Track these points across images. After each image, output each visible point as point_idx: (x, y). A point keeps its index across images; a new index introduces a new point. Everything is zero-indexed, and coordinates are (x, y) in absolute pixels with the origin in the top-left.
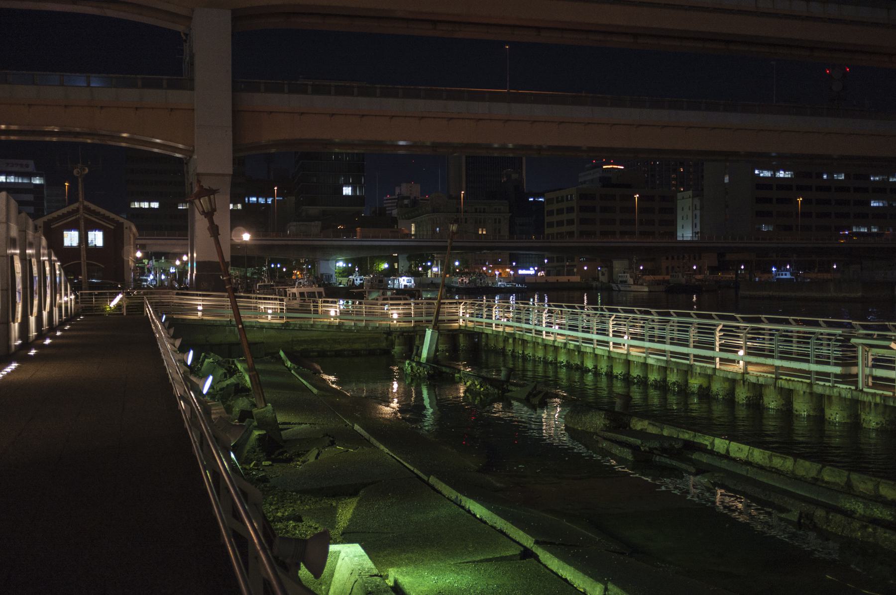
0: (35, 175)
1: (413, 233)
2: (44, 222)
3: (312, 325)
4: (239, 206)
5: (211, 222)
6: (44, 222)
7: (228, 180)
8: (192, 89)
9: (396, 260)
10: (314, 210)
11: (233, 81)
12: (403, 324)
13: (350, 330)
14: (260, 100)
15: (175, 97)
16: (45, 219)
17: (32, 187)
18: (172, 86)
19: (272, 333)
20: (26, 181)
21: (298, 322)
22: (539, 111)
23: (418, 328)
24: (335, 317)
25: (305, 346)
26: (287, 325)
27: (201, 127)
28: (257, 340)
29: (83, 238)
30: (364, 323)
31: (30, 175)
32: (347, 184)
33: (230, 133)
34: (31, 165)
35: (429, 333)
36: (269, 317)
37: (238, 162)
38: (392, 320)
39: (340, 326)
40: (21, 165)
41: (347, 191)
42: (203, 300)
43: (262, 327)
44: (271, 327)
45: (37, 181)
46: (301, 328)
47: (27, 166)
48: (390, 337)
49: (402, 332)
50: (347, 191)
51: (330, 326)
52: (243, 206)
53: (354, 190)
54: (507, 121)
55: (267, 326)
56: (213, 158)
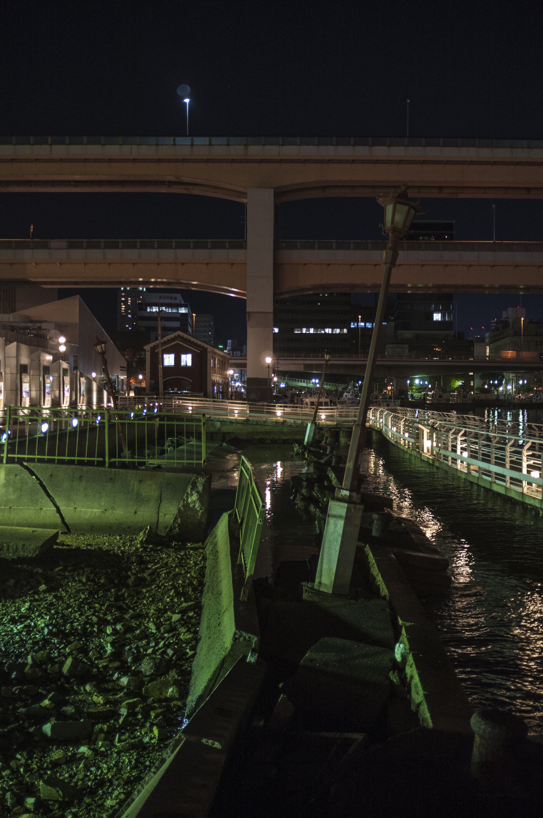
0: (182, 306)
1: (488, 354)
2: (151, 348)
3: (265, 422)
4: (345, 331)
5: (103, 357)
6: (151, 348)
7: (271, 316)
8: (246, 249)
9: (472, 378)
10: (408, 334)
11: (275, 241)
12: (329, 423)
13: (291, 426)
14: (295, 255)
15: (235, 255)
16: (152, 345)
17: (179, 316)
18: (233, 246)
19: (240, 426)
20: (174, 311)
21: (255, 419)
22: (519, 257)
23: (339, 426)
24: (281, 417)
25: (262, 436)
26: (247, 421)
27: (247, 276)
28: (229, 431)
29: (178, 360)
30: (300, 422)
31: (178, 306)
32: (437, 311)
33: (272, 282)
34: (180, 299)
35: (309, 425)
36: (236, 415)
37: (276, 302)
38: (322, 420)
39: (284, 422)
40: (171, 298)
41: (437, 317)
42: (192, 403)
43: (231, 422)
44: (237, 422)
45: (183, 311)
46: (257, 423)
47: (175, 298)
48: (321, 432)
49: (329, 428)
50: (437, 317)
51: (277, 422)
52: (348, 331)
53: (443, 316)
54: (494, 266)
55: (234, 421)
56: (260, 300)
